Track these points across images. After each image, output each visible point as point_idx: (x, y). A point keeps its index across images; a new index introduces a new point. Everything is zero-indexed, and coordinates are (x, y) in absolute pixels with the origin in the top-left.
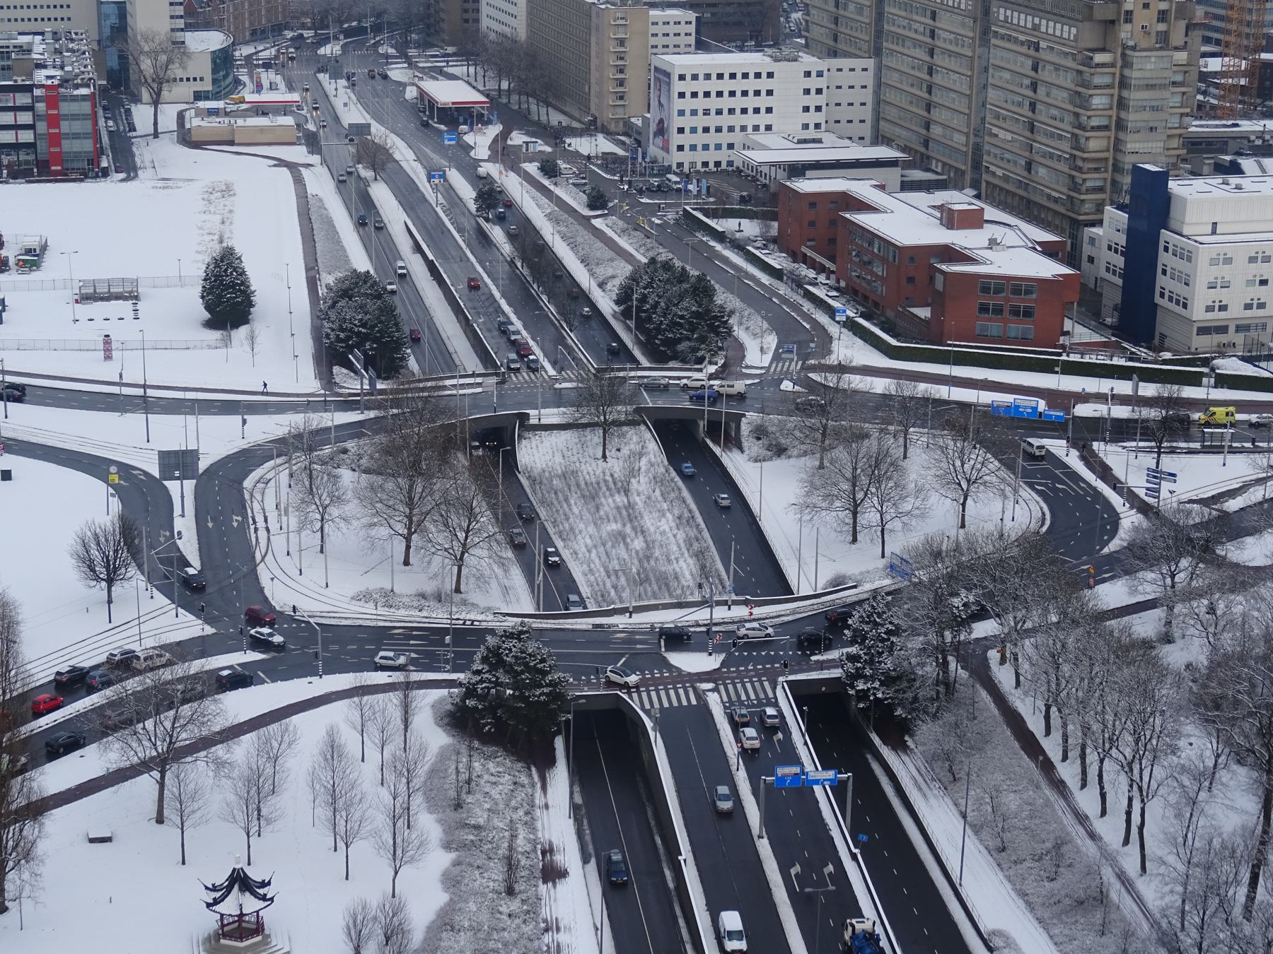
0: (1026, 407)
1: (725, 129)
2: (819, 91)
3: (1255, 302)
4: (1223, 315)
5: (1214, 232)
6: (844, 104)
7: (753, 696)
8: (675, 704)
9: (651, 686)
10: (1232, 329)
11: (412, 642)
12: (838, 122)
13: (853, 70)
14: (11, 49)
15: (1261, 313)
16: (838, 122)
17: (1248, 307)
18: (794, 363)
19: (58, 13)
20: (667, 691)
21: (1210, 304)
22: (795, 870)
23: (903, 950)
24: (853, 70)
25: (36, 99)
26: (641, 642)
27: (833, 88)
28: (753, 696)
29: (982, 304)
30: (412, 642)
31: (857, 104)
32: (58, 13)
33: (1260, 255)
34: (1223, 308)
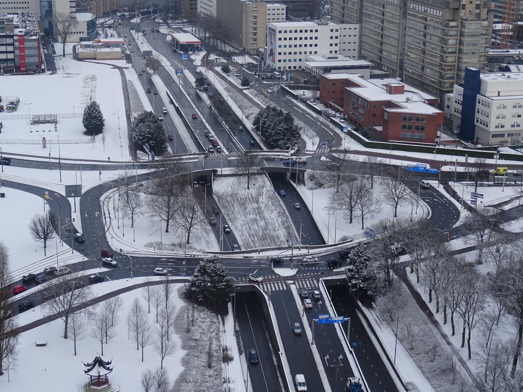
0: (421, 167)
1: (298, 53)
2: (336, 38)
3: (516, 124)
4: (502, 129)
5: (499, 95)
6: (347, 43)
7: (309, 286)
8: (277, 289)
9: (268, 282)
10: (506, 135)
11: (169, 264)
12: (344, 50)
13: (350, 29)
14: (5, 20)
15: (518, 128)
16: (344, 50)
17: (513, 126)
18: (326, 149)
19: (24, 5)
20: (274, 284)
21: (497, 125)
22: (326, 358)
23: (371, 390)
24: (350, 29)
25: (15, 41)
26: (263, 264)
27: (342, 36)
28: (309, 286)
29: (403, 125)
30: (169, 264)
31: (352, 43)
32: (24, 5)
33: (518, 105)
34: (502, 127)
